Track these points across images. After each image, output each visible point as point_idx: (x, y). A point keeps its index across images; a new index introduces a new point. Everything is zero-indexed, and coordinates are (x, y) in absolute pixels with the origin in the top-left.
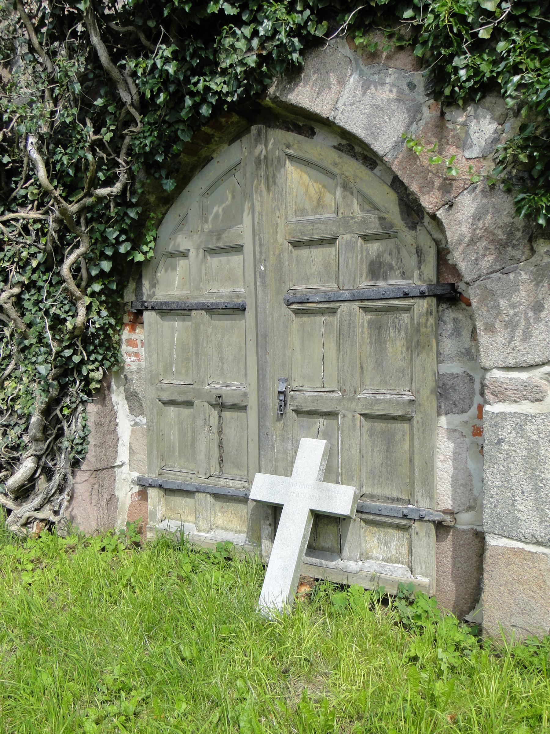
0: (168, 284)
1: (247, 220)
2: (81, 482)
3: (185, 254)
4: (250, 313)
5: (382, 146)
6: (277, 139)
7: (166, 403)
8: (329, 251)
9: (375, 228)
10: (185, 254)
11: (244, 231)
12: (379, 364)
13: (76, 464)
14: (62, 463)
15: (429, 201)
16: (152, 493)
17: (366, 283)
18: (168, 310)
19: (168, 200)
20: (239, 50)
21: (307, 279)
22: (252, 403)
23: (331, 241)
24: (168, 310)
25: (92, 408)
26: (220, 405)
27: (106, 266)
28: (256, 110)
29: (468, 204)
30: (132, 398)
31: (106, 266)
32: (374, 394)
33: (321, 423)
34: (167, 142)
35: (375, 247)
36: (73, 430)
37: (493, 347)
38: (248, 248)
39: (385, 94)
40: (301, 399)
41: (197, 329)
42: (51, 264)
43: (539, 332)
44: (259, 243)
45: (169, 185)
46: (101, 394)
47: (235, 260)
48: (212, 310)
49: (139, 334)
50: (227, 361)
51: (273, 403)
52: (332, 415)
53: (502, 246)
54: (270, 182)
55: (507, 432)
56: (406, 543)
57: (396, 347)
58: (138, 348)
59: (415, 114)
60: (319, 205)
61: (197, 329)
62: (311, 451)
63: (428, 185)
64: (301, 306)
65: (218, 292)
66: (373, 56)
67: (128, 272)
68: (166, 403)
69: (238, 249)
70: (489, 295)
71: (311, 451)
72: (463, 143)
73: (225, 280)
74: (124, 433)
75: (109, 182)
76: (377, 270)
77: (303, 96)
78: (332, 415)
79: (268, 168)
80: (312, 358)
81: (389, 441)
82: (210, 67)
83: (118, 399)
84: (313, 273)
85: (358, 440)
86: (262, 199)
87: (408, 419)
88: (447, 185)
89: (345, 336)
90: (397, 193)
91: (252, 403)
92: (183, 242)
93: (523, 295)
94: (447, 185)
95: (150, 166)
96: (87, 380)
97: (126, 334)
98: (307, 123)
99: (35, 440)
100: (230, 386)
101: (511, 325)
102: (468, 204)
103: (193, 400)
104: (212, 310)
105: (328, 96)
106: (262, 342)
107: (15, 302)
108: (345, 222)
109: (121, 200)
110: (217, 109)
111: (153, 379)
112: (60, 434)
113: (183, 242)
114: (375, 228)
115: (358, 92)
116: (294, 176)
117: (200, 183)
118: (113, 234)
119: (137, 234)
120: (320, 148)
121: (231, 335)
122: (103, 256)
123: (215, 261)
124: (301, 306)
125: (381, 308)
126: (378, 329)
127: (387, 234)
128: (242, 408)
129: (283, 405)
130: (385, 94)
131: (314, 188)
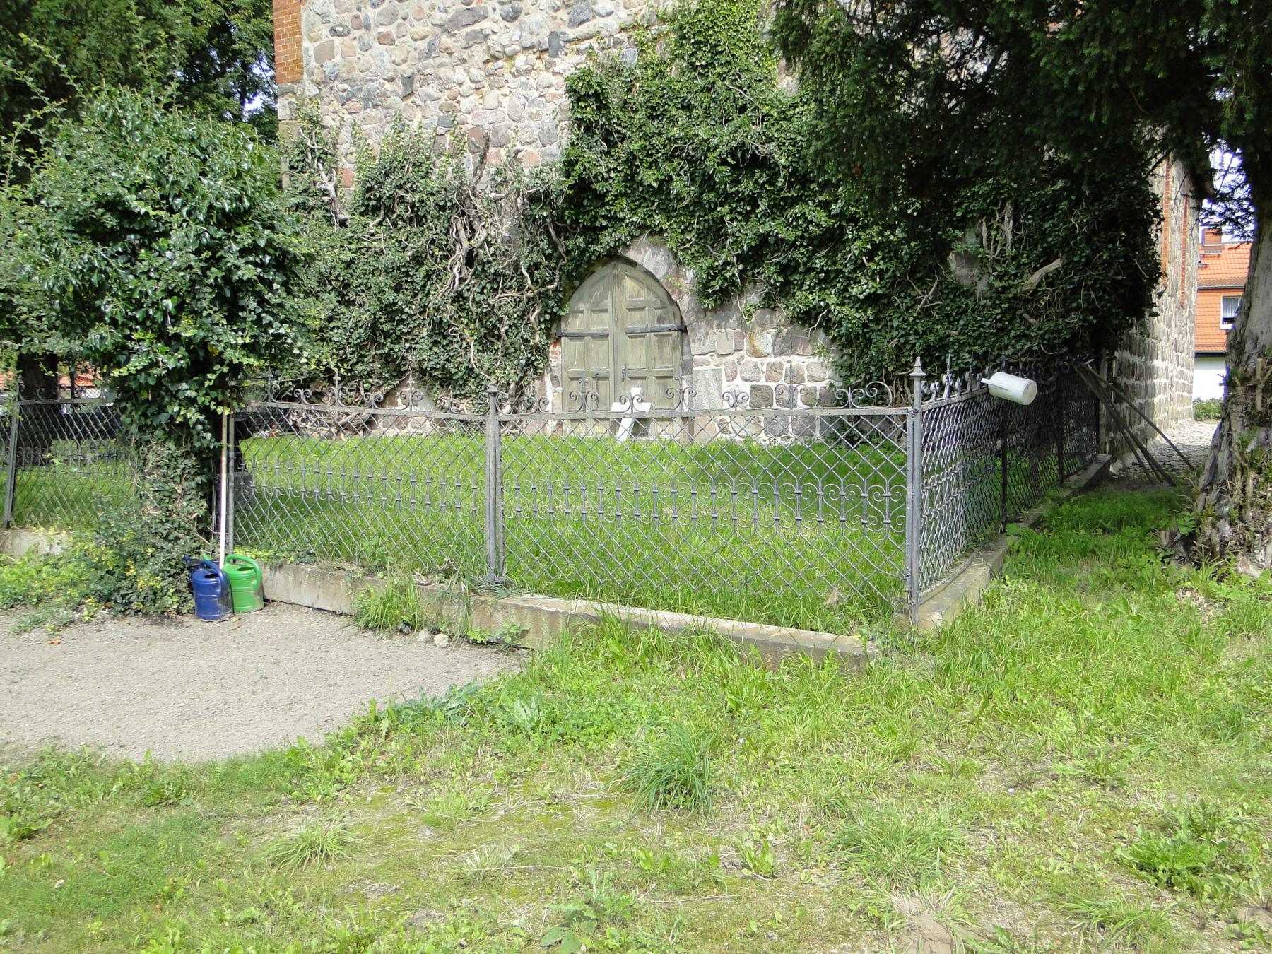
0: (574, 325)
1: (609, 298)
3: (582, 312)
4: (610, 338)
6: (621, 267)
7: (572, 379)
8: (643, 312)
9: (659, 305)
10: (582, 312)
11: (608, 303)
12: (661, 357)
14: (522, 408)
15: (674, 297)
17: (656, 325)
18: (573, 337)
19: (574, 289)
21: (633, 323)
22: (612, 375)
23: (643, 309)
24: (573, 337)
25: (537, 382)
26: (598, 378)
27: (548, 317)
28: (613, 256)
29: (686, 298)
30: (554, 379)
31: (548, 317)
32: (661, 368)
33: (640, 382)
34: (577, 267)
35: (659, 311)
36: (528, 392)
38: (610, 310)
39: (660, 258)
41: (587, 345)
42: (524, 313)
43: (708, 342)
44: (614, 309)
45: (577, 283)
46: (540, 376)
47: (605, 315)
48: (595, 336)
49: (558, 348)
50: (600, 359)
51: (620, 374)
52: (644, 378)
53: (697, 313)
54: (619, 284)
55: (700, 377)
57: (667, 349)
58: (558, 355)
59: (670, 266)
60: (638, 295)
61: (587, 345)
63: (674, 291)
64: (632, 335)
65: (596, 328)
66: (656, 245)
67: (556, 319)
68: (572, 379)
69: (606, 311)
70: (693, 330)
72: (685, 278)
73: (600, 323)
74: (550, 392)
75: (551, 282)
76: (660, 320)
77: (631, 255)
78: (644, 378)
79: (618, 279)
80: (637, 356)
81: (665, 385)
82: (596, 241)
83: (547, 379)
84: (637, 321)
85: (654, 387)
86: (616, 291)
87: (671, 377)
88: (680, 292)
89: (649, 346)
91: (612, 375)
92: (582, 306)
93: (703, 329)
94: (680, 292)
95: (569, 276)
96: (536, 368)
97: (552, 348)
98: (633, 264)
99: (511, 396)
100: (602, 369)
101: (700, 340)
102: (686, 298)
104: (595, 336)
105: (640, 256)
106: (615, 350)
107: (1204, 181)
108: (648, 301)
109: (556, 290)
110: (598, 257)
111: (564, 368)
112: (523, 394)
113: (582, 306)
114: (659, 305)
115: (648, 256)
116: (628, 282)
117: (588, 282)
118: (552, 303)
119: (561, 303)
122: (546, 312)
123: (595, 315)
124: (632, 335)
125: (661, 335)
126: (660, 343)
127: (663, 307)
128: (607, 378)
129: (624, 375)
130: (660, 258)
131: (636, 287)
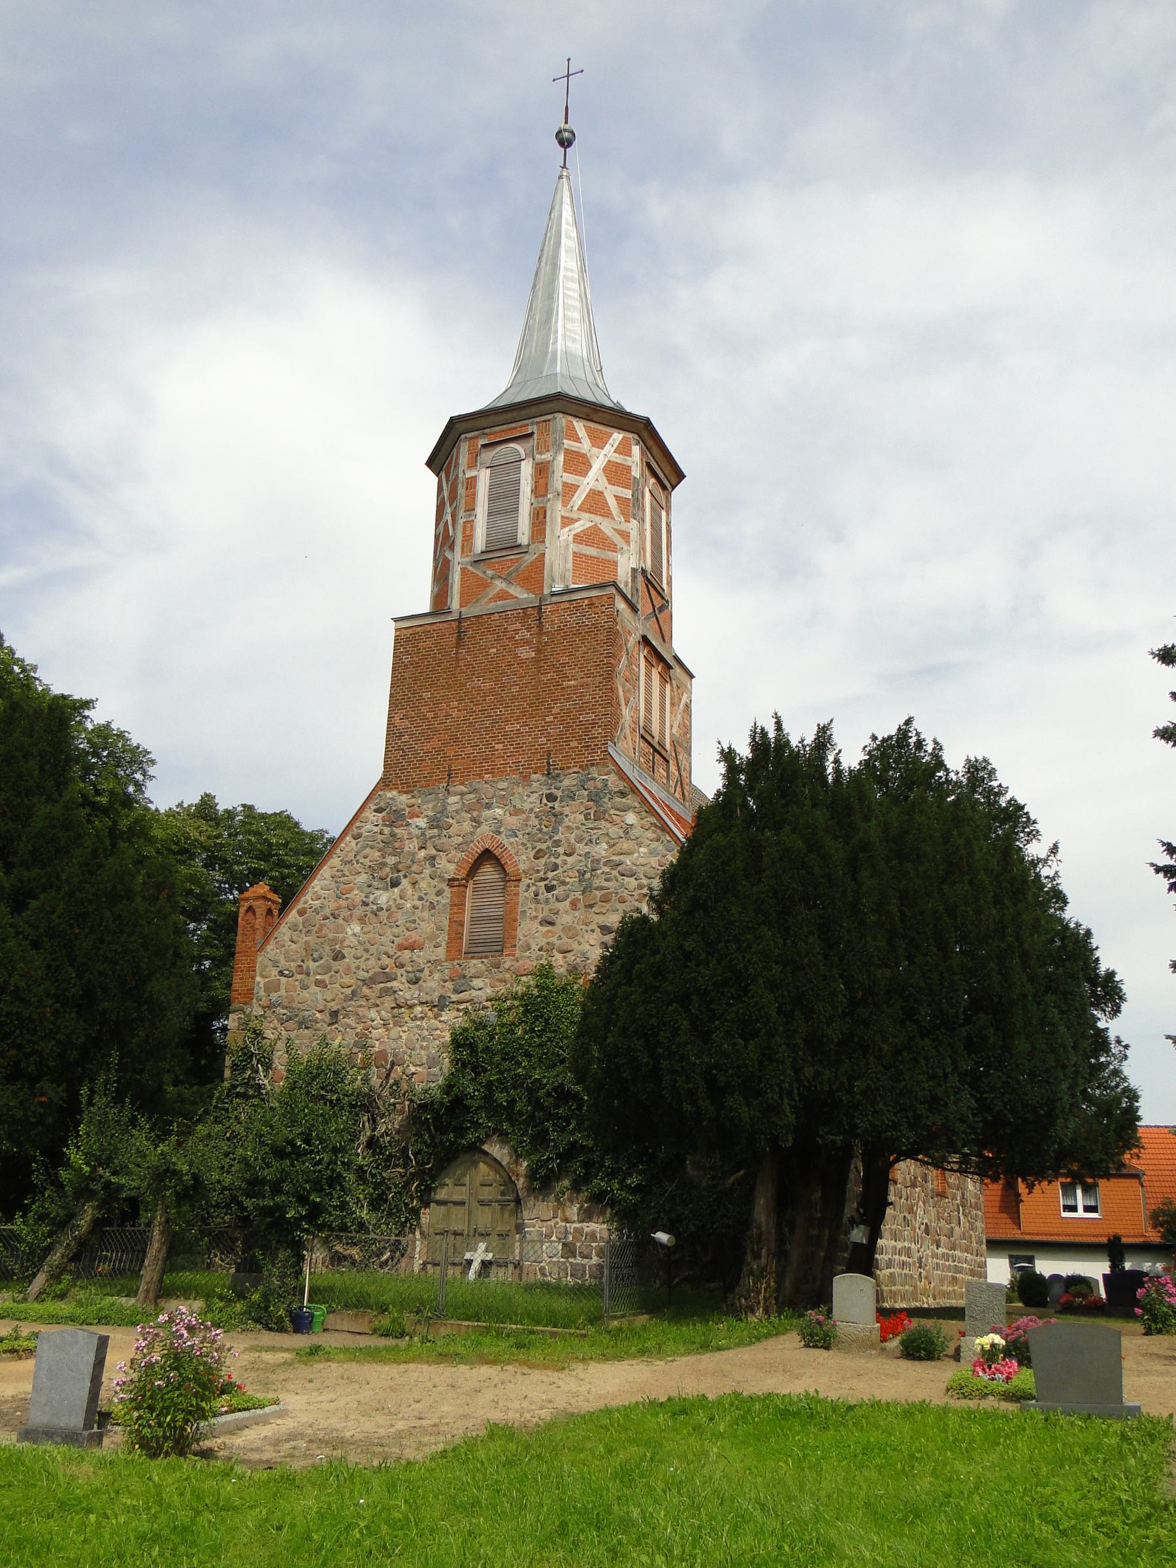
0: (442, 1194)
2: (404, 1262)
5: (504, 1163)
11: (467, 1180)
13: (403, 1255)
16: (429, 1266)
20: (471, 1136)
22: (465, 1233)
26: (455, 1234)
37: (526, 1214)
40: (482, 1230)
47: (463, 1188)
48: (456, 1203)
49: (428, 1211)
56: (103, 1394)
61: (448, 1210)
62: (482, 1246)
64: (482, 1203)
65: (457, 1197)
67: (429, 1189)
71: (482, 1246)
73: (460, 1194)
76: (503, 1194)
77: (485, 1147)
79: (475, 1164)
84: (486, 1193)
89: (494, 1212)
90: (263, 816)
92: (447, 1181)
98: (486, 1154)
100: (458, 1227)
102: (522, 1180)
103: (1034, 1362)
104: (456, 1203)
108: (495, 1180)
109: (430, 1169)
113: (447, 1181)
115: (497, 1150)
116: (482, 1166)
120: (488, 1160)
121: (460, 1212)
124: (482, 1203)
130: (505, 1151)
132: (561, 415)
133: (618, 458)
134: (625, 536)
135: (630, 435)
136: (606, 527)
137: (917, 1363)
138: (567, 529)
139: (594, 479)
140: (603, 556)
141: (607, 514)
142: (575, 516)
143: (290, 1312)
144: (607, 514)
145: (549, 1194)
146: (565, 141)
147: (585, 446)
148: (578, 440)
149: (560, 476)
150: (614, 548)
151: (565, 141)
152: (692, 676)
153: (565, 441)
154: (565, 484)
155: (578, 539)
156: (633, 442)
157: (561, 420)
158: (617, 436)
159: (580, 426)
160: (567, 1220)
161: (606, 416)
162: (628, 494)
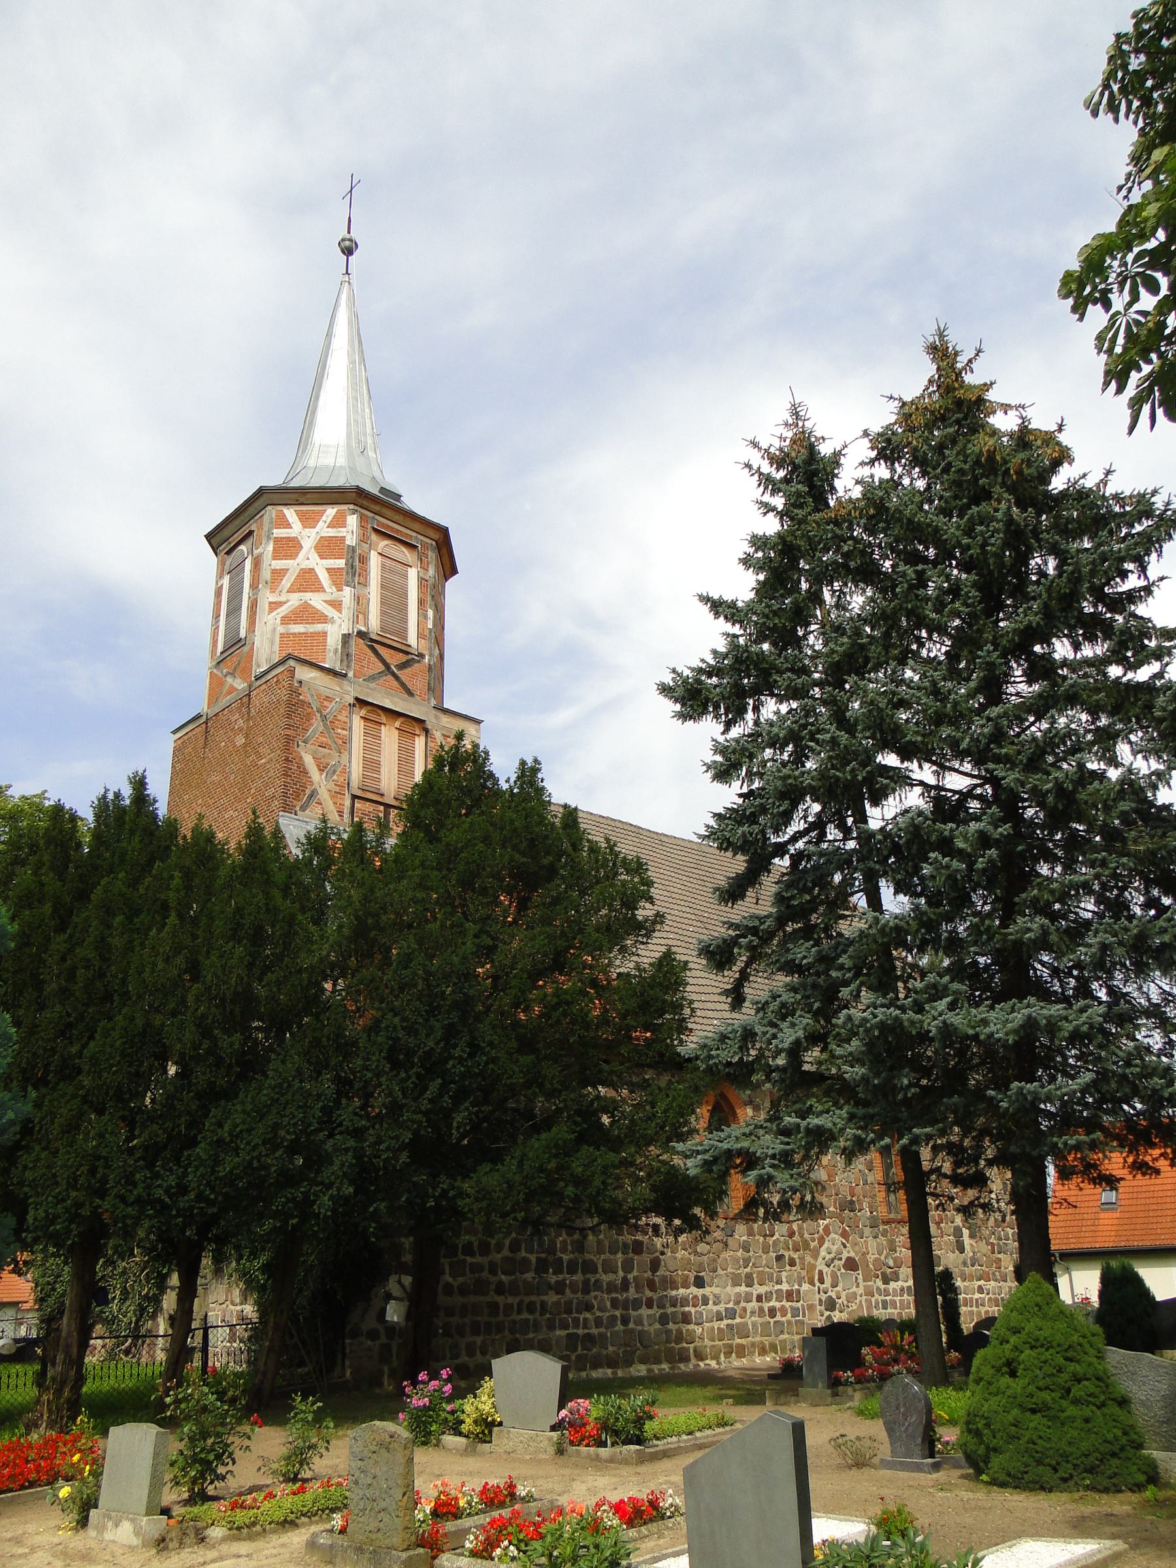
132: (269, 508)
133: (332, 532)
134: (336, 605)
135: (345, 507)
136: (316, 601)
137: (1042, 1496)
138: (275, 613)
139: (307, 558)
140: (311, 630)
141: (319, 588)
142: (283, 599)
143: (622, 1316)
144: (319, 588)
145: (222, 1278)
146: (348, 251)
147: (296, 528)
148: (289, 526)
149: (271, 563)
150: (324, 619)
151: (348, 251)
152: (478, 722)
153: (275, 531)
154: (274, 572)
155: (286, 620)
156: (347, 512)
157: (271, 512)
158: (331, 512)
159: (290, 513)
160: (233, 1304)
161: (316, 495)
162: (341, 563)
